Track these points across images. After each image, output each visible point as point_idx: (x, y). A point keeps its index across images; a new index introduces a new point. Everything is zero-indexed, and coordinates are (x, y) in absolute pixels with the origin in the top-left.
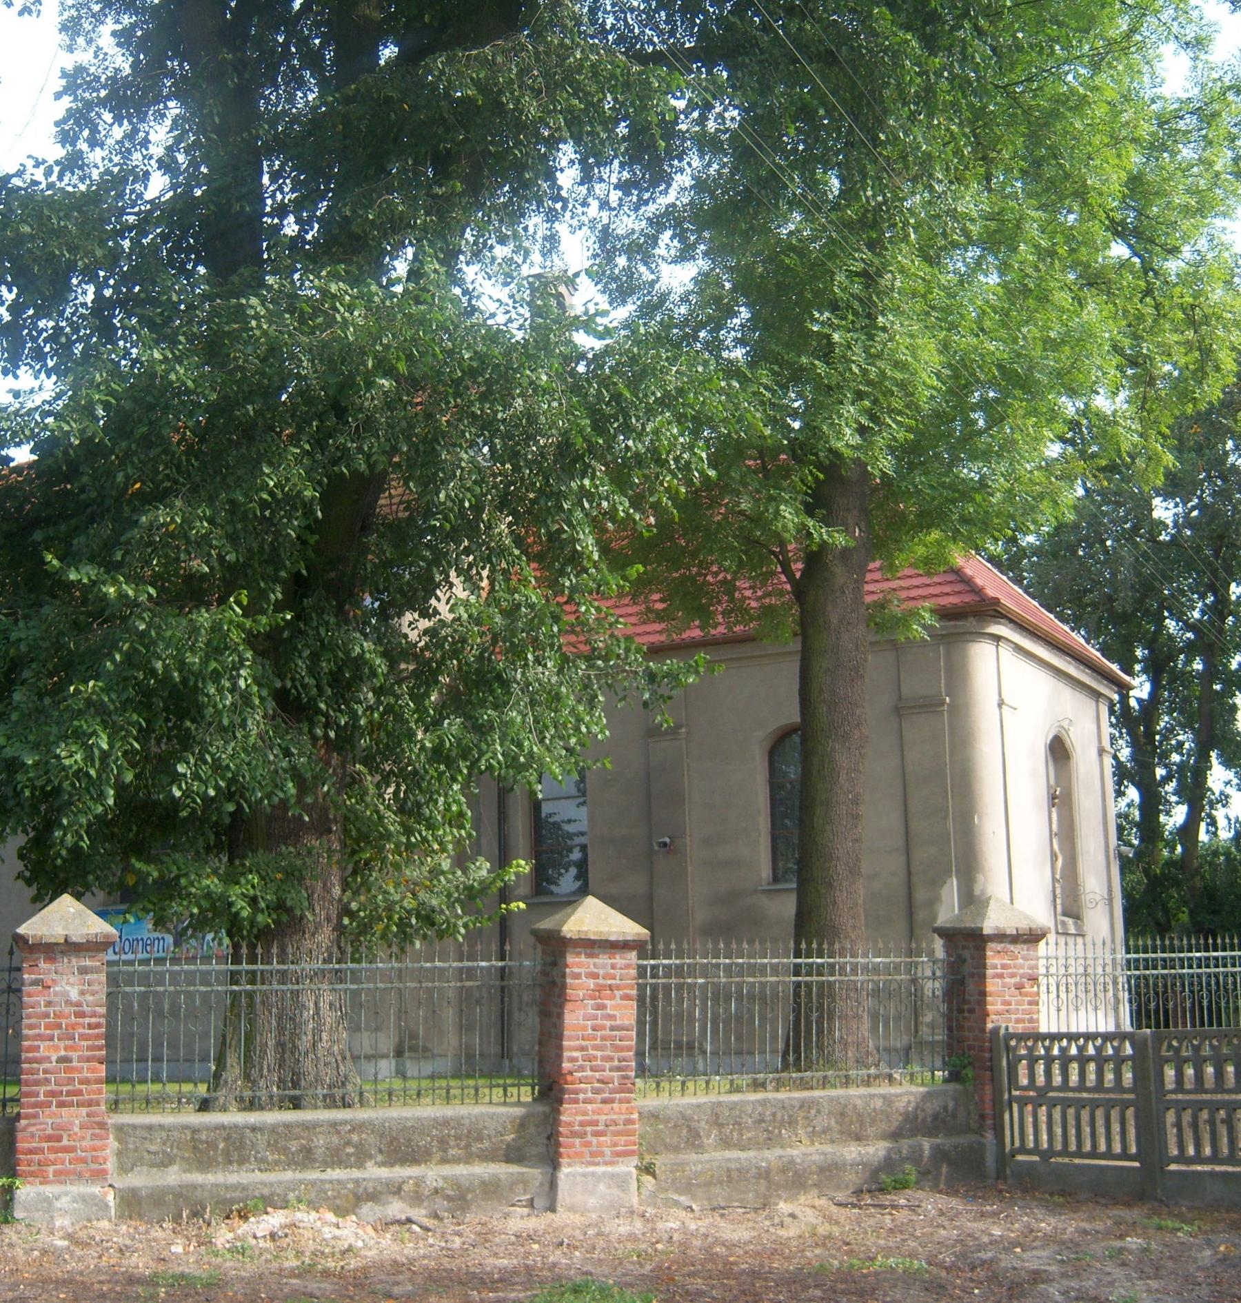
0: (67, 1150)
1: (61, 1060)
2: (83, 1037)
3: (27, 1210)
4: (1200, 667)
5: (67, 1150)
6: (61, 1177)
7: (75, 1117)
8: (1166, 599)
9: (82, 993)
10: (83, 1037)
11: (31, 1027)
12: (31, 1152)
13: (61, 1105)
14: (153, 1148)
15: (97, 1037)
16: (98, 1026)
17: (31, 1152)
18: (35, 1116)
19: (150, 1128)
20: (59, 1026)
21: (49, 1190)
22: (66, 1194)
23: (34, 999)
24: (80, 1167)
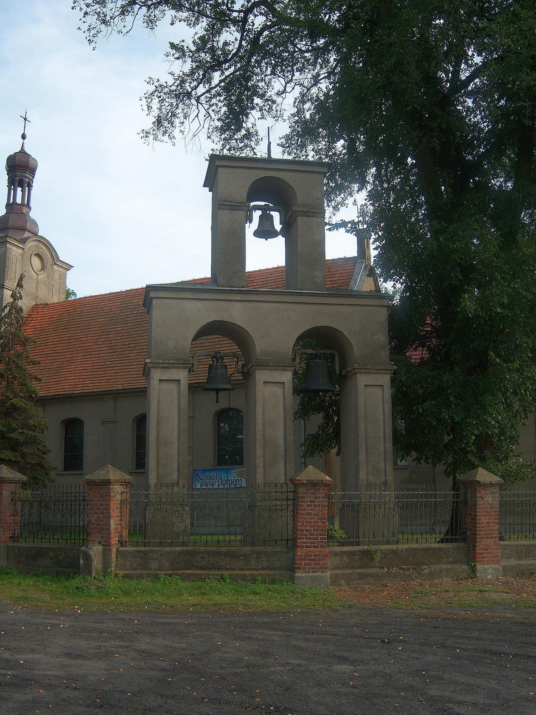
0: (490, 553)
1: (488, 523)
2: (493, 515)
3: (480, 573)
4: (409, 159)
5: (490, 553)
6: (488, 562)
7: (490, 542)
8: (281, 19)
9: (493, 500)
10: (493, 515)
11: (479, 512)
12: (480, 554)
13: (487, 538)
14: (507, 552)
15: (497, 515)
16: (497, 511)
17: (480, 554)
18: (480, 542)
19: (506, 545)
20: (319, 564)
21: (486, 566)
22: (490, 568)
23: (480, 502)
24: (493, 559)
